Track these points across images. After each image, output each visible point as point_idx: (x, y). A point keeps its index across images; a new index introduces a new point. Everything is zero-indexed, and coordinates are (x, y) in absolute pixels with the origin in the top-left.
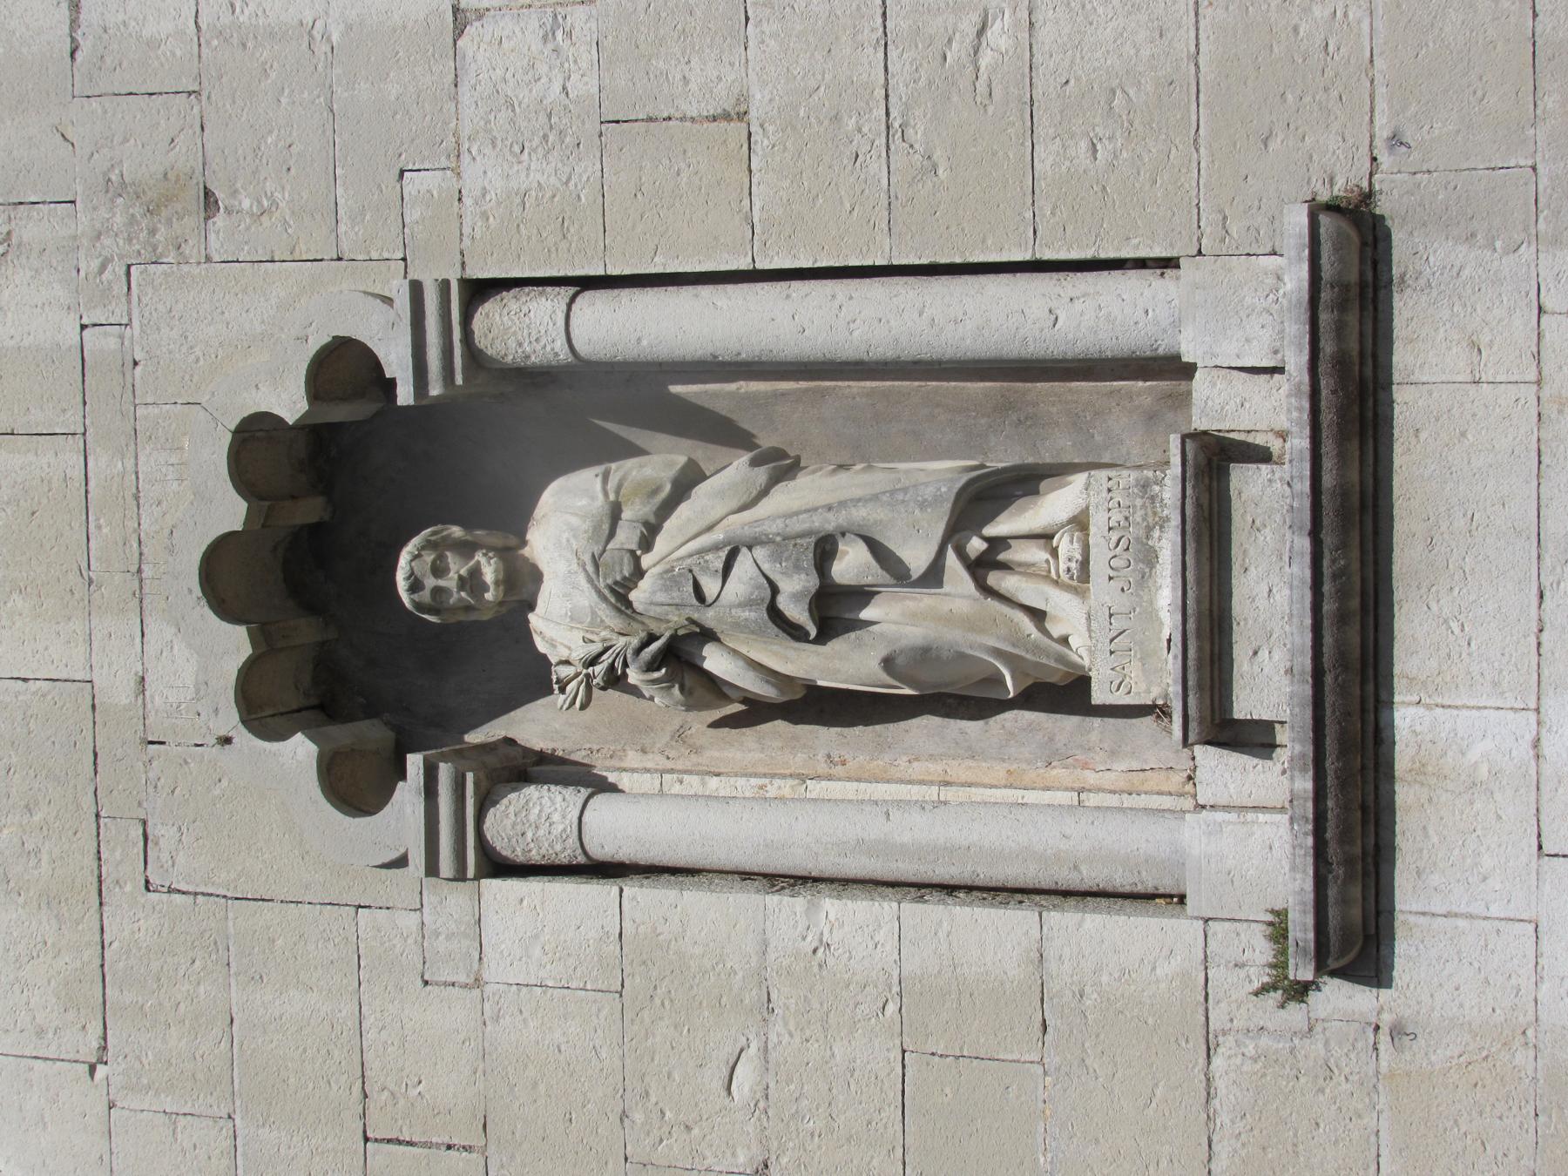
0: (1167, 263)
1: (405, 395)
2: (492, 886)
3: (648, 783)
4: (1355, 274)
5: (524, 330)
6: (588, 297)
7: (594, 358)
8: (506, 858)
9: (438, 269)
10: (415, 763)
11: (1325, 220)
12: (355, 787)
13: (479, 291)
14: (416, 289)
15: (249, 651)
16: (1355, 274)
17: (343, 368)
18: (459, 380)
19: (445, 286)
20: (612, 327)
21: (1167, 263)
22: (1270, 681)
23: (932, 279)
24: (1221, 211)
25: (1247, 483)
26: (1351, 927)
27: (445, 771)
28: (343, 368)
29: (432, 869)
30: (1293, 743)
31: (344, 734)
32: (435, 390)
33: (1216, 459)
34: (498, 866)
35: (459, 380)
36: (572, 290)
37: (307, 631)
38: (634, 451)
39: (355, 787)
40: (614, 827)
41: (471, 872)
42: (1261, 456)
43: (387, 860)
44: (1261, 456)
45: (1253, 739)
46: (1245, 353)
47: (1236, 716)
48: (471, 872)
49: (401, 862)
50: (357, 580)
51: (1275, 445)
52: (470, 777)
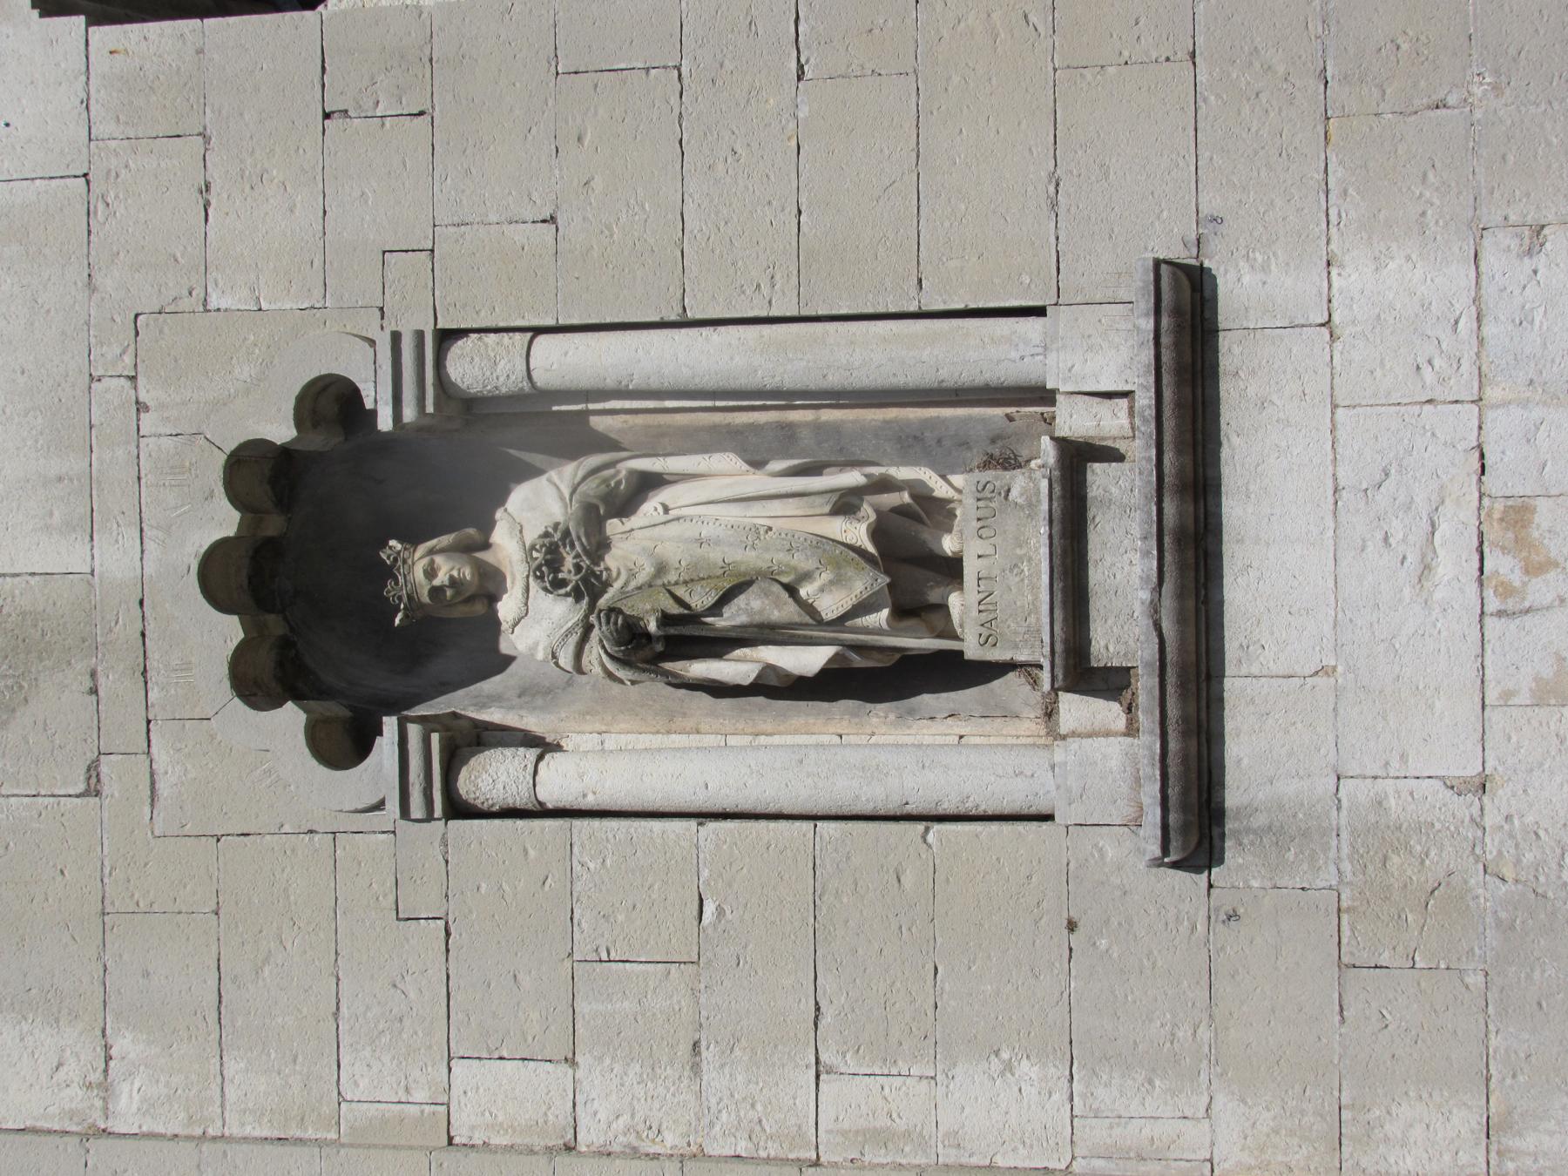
0: (1040, 312)
1: (385, 423)
2: (454, 824)
3: (589, 741)
4: (1188, 314)
5: (477, 368)
6: (542, 340)
7: (549, 387)
8: (466, 802)
9: (415, 320)
10: (390, 724)
11: (1164, 267)
12: (343, 743)
13: (447, 337)
14: (396, 337)
15: (241, 635)
16: (1188, 314)
17: (332, 403)
18: (430, 409)
19: (420, 335)
20: (560, 362)
21: (1040, 312)
22: (1125, 624)
23: (1022, 319)
24: (1364, 541)
25: (1099, 476)
26: (1197, 822)
27: (414, 731)
28: (332, 403)
29: (405, 812)
30: (1145, 686)
31: (319, 706)
32: (409, 414)
33: (1078, 457)
34: (458, 809)
35: (430, 409)
36: (529, 335)
37: (275, 625)
38: (536, 472)
39: (343, 743)
40: (559, 781)
41: (438, 812)
42: (1111, 455)
43: (360, 807)
44: (1111, 455)
45: (1107, 682)
46: (1100, 365)
47: (1094, 664)
48: (438, 812)
49: (380, 806)
50: (341, 576)
51: (1122, 446)
52: (435, 737)
